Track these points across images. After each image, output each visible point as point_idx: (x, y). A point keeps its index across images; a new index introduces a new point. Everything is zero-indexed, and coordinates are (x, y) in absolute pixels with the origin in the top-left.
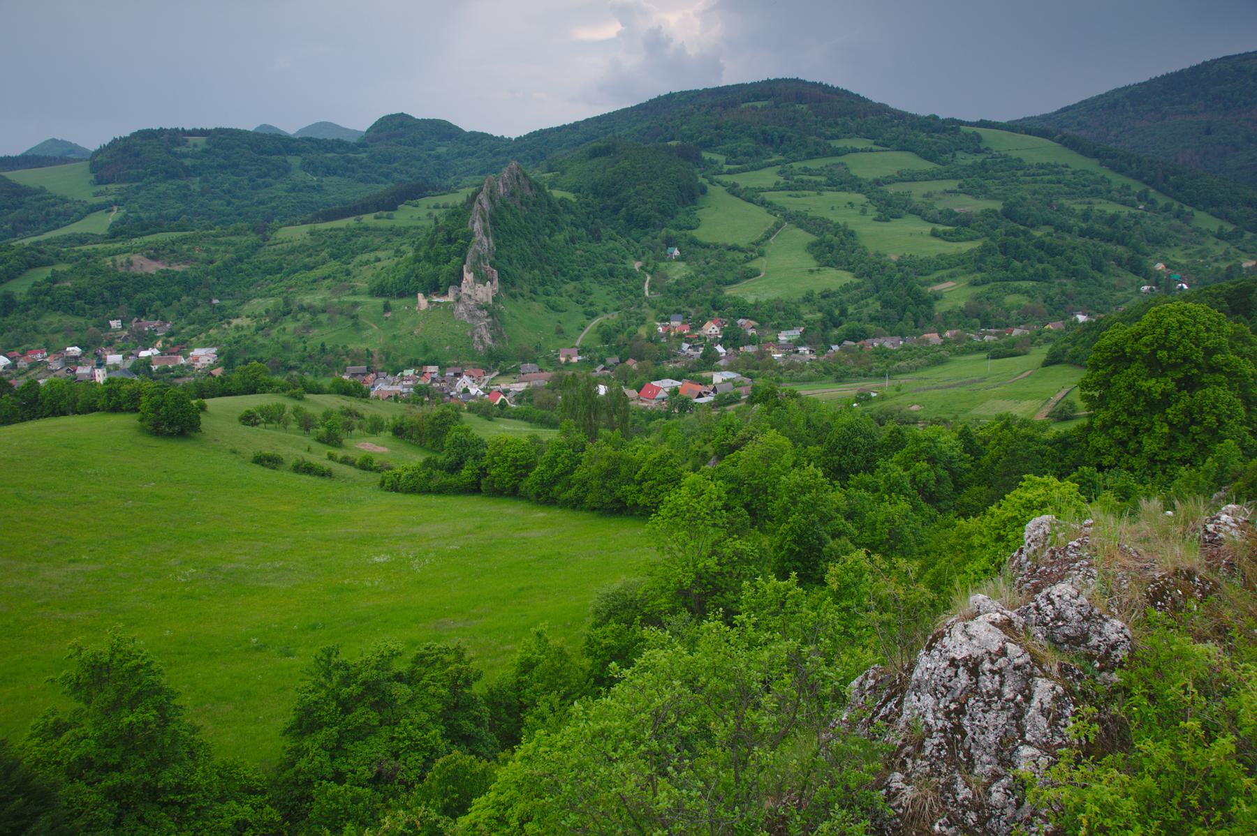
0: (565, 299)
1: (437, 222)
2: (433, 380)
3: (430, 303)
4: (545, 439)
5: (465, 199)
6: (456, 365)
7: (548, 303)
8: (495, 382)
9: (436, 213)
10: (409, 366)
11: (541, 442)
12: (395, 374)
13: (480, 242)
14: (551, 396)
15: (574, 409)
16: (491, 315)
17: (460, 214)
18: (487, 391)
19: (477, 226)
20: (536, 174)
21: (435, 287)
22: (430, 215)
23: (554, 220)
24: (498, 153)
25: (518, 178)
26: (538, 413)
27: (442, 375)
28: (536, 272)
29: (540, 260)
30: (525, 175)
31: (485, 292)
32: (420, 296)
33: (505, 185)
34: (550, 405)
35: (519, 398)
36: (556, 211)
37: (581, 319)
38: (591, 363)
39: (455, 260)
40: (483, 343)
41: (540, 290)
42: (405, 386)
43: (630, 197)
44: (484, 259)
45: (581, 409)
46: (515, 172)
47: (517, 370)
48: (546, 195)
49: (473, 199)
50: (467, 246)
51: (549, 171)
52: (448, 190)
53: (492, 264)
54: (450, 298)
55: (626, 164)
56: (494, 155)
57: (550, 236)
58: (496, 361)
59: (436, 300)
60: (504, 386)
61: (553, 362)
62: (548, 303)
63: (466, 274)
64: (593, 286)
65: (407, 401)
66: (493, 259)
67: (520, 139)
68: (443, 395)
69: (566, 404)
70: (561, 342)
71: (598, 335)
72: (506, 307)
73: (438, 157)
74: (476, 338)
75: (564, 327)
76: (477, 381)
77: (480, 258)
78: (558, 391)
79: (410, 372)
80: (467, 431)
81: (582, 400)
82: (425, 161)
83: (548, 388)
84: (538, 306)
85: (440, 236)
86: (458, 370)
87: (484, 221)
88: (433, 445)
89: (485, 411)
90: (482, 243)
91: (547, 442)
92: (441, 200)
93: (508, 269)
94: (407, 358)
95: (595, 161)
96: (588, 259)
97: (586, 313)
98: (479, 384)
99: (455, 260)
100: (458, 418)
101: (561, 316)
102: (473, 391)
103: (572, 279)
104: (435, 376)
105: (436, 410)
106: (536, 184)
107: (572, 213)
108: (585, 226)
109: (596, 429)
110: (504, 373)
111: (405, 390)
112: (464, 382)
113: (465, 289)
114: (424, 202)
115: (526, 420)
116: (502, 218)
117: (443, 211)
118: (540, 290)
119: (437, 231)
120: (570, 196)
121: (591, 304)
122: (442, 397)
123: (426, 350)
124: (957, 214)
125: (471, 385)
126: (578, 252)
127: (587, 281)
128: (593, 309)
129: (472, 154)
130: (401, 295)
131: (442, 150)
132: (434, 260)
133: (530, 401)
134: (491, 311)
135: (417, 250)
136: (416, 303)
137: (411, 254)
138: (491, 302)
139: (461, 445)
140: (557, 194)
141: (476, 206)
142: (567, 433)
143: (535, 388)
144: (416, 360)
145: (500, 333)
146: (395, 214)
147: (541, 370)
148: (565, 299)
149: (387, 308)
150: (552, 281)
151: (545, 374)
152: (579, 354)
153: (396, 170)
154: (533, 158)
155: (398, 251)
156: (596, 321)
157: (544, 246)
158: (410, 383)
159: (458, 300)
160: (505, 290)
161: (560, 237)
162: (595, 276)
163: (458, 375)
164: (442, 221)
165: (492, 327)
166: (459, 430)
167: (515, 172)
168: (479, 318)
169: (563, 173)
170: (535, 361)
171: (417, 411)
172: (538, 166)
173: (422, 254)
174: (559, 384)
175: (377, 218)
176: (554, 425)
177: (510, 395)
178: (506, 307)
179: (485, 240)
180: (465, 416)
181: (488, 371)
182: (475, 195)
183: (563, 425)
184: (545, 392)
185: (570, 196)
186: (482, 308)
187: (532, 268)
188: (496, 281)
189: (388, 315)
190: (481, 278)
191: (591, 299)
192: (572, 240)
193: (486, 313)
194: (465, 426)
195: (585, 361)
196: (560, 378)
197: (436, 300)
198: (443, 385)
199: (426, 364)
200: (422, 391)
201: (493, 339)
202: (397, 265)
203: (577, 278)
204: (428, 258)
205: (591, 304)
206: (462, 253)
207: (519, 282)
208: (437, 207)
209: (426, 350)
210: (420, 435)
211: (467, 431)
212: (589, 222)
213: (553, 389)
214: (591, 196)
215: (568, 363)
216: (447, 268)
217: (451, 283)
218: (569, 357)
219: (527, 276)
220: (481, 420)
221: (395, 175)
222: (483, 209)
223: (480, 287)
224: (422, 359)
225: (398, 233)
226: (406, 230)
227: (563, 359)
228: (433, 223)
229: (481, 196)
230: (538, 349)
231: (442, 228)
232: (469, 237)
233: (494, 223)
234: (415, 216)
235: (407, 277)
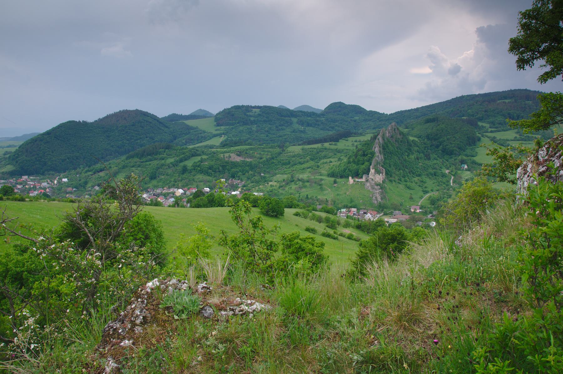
32: (350, 178)
43: (444, 141)
54: (363, 180)
55: (443, 126)
72: (388, 185)
149: (335, 182)
168: (376, 189)
175: (330, 144)
189: (335, 185)
193: (379, 187)
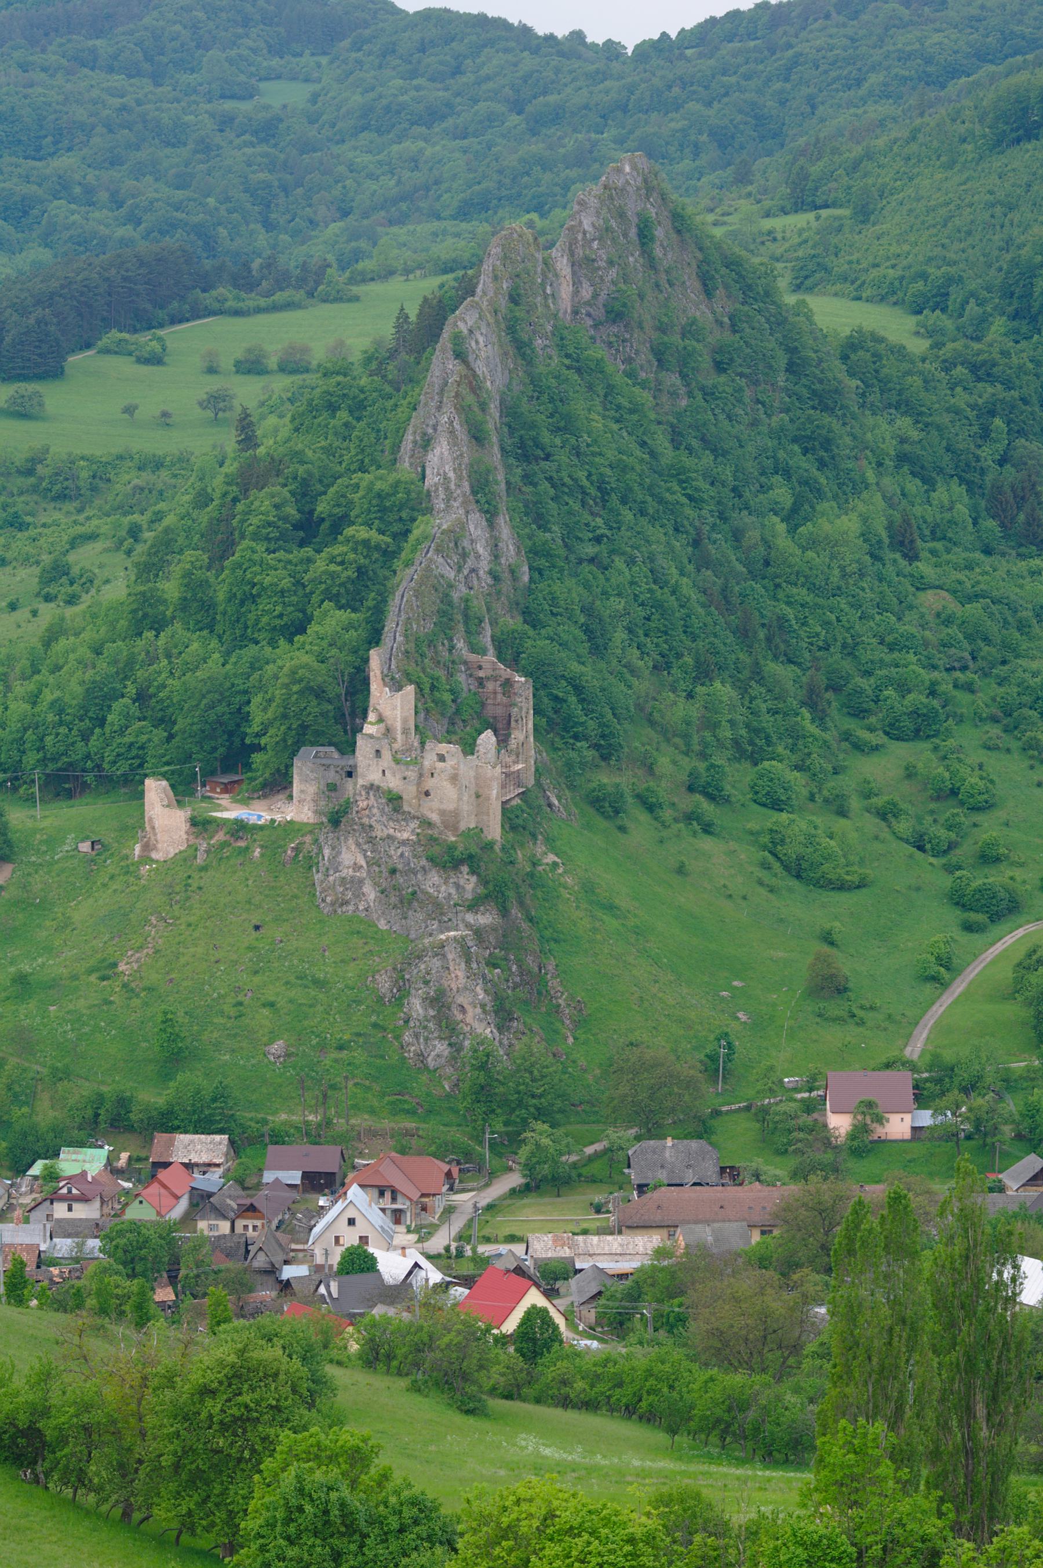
0: (857, 828)
1: (248, 439)
2: (202, 1202)
3: (200, 825)
4: (739, 1517)
5: (387, 330)
6: (314, 1136)
7: (774, 844)
8: (504, 1224)
9: (248, 392)
10: (90, 1129)
11: (719, 1529)
12: (20, 1169)
13: (455, 542)
14: (778, 1303)
15: (886, 1372)
16: (494, 894)
17: (356, 405)
18: (460, 1266)
19: (442, 463)
20: (735, 218)
21: (226, 754)
22: (216, 402)
23: (817, 445)
24: (556, 116)
25: (645, 235)
26: (710, 1385)
27: (245, 1181)
28: (723, 690)
29: (744, 634)
30: (680, 223)
31: (467, 784)
33: (583, 265)
34: (772, 1346)
35: (620, 1306)
36: (825, 399)
37: (936, 926)
38: (982, 1142)
39: (331, 621)
40: (450, 1030)
41: (738, 777)
42: (62, 1229)
44: (472, 623)
45: (926, 1372)
46: (632, 207)
47: (611, 1168)
48: (779, 321)
49: (428, 328)
50: (389, 555)
51: (799, 204)
52: (311, 285)
53: (509, 650)
54: (299, 808)
56: (536, 126)
57: (794, 517)
58: (509, 1124)
59: (230, 811)
60: (544, 1247)
61: (792, 1135)
62: (774, 844)
63: (379, 694)
64: (995, 763)
65: (66, 1301)
66: (513, 622)
67: (659, 48)
68: (248, 1280)
69: (851, 1345)
70: (834, 1036)
71: (1015, 1011)
72: (572, 857)
73: (267, 130)
74: (417, 1007)
75: (845, 965)
76: (409, 1213)
77: (450, 615)
78: (811, 1279)
79: (86, 1161)
80: (357, 1458)
81: (930, 1326)
82: (205, 148)
83: (763, 1262)
84: (725, 860)
85: (265, 503)
86: (326, 1159)
87: (478, 437)
88: (188, 1525)
89: (450, 1368)
90: (464, 540)
91: (752, 1533)
92: (275, 332)
93: (588, 672)
94: (80, 1091)
95: (1024, 158)
96: (976, 635)
97: (959, 900)
98: (424, 1232)
99: (331, 621)
100: (313, 1392)
101: (833, 911)
102: (392, 1266)
103: (894, 732)
104: (212, 1180)
105: (212, 1352)
106: (732, 264)
107: (904, 405)
108: (966, 472)
109: (998, 1477)
110: (545, 1183)
111: (64, 1246)
112: (352, 1216)
113: (373, 766)
114: (189, 340)
115: (649, 1418)
116: (565, 426)
117: (281, 384)
118: (738, 777)
119: (248, 480)
120: (896, 326)
121: (988, 858)
122: (240, 1286)
123: (175, 1056)
124: (578, 1355)
125: (380, 1236)
126: (931, 601)
127: (967, 739)
128: (995, 878)
129: (432, 116)
130: (65, 783)
131: (284, 96)
132: (227, 618)
133: (672, 1324)
134: (497, 874)
135: (151, 569)
136: (136, 825)
137: (117, 589)
138: (494, 831)
139: (323, 1529)
140: (834, 315)
141: (441, 365)
142: (848, 1490)
143: (698, 1252)
144: (123, 1103)
145: (534, 986)
146: (53, 396)
147: (730, 1174)
148: (857, 828)
150: (795, 735)
151: (750, 1192)
152: (921, 1098)
153: (62, 188)
154: (723, 139)
155: (58, 572)
156: (1011, 940)
157: (765, 567)
158: (82, 1212)
159: (337, 819)
160: (569, 775)
161: (842, 524)
162: (1007, 717)
163: (323, 1182)
164: (274, 433)
165: (499, 951)
166: (318, 1455)
167: (632, 207)
168: (437, 910)
169: (864, 214)
170: (701, 1128)
171: (119, 1349)
172: (743, 178)
173: (171, 589)
174: (816, 1245)
176: (788, 1449)
177: (574, 1290)
178: (572, 857)
179: (476, 527)
180: (351, 1384)
181: (467, 1168)
182: (436, 316)
183: (834, 1449)
184: (746, 1284)
185: (896, 326)
186: (450, 861)
187: (703, 673)
188: (523, 733)
190: (454, 715)
191: (989, 829)
192: (903, 541)
193: (470, 884)
194: (349, 1435)
195: (951, 1136)
196: (825, 1214)
197: (230, 811)
198: (250, 1228)
199: (168, 1122)
200: (146, 1258)
201: (502, 1014)
202: (49, 640)
203: (921, 727)
204: (199, 609)
205: (988, 858)
206: (363, 591)
207: (637, 739)
208: (252, 366)
209: (175, 1056)
210: (124, 1470)
211: (357, 1458)
212: (988, 454)
213: (788, 1266)
214: (999, 325)
215: (864, 1145)
216: (293, 659)
217: (302, 736)
218: (870, 1112)
219: (679, 710)
220: (431, 1410)
221: (58, 208)
222: (474, 383)
223: (444, 758)
224: (153, 1097)
225: (66, 486)
226: (101, 475)
227: (840, 1123)
228: (229, 440)
229: (464, 320)
230: (718, 1067)
231: (275, 467)
232: (400, 513)
233: (525, 450)
234: (149, 409)
235: (98, 702)
